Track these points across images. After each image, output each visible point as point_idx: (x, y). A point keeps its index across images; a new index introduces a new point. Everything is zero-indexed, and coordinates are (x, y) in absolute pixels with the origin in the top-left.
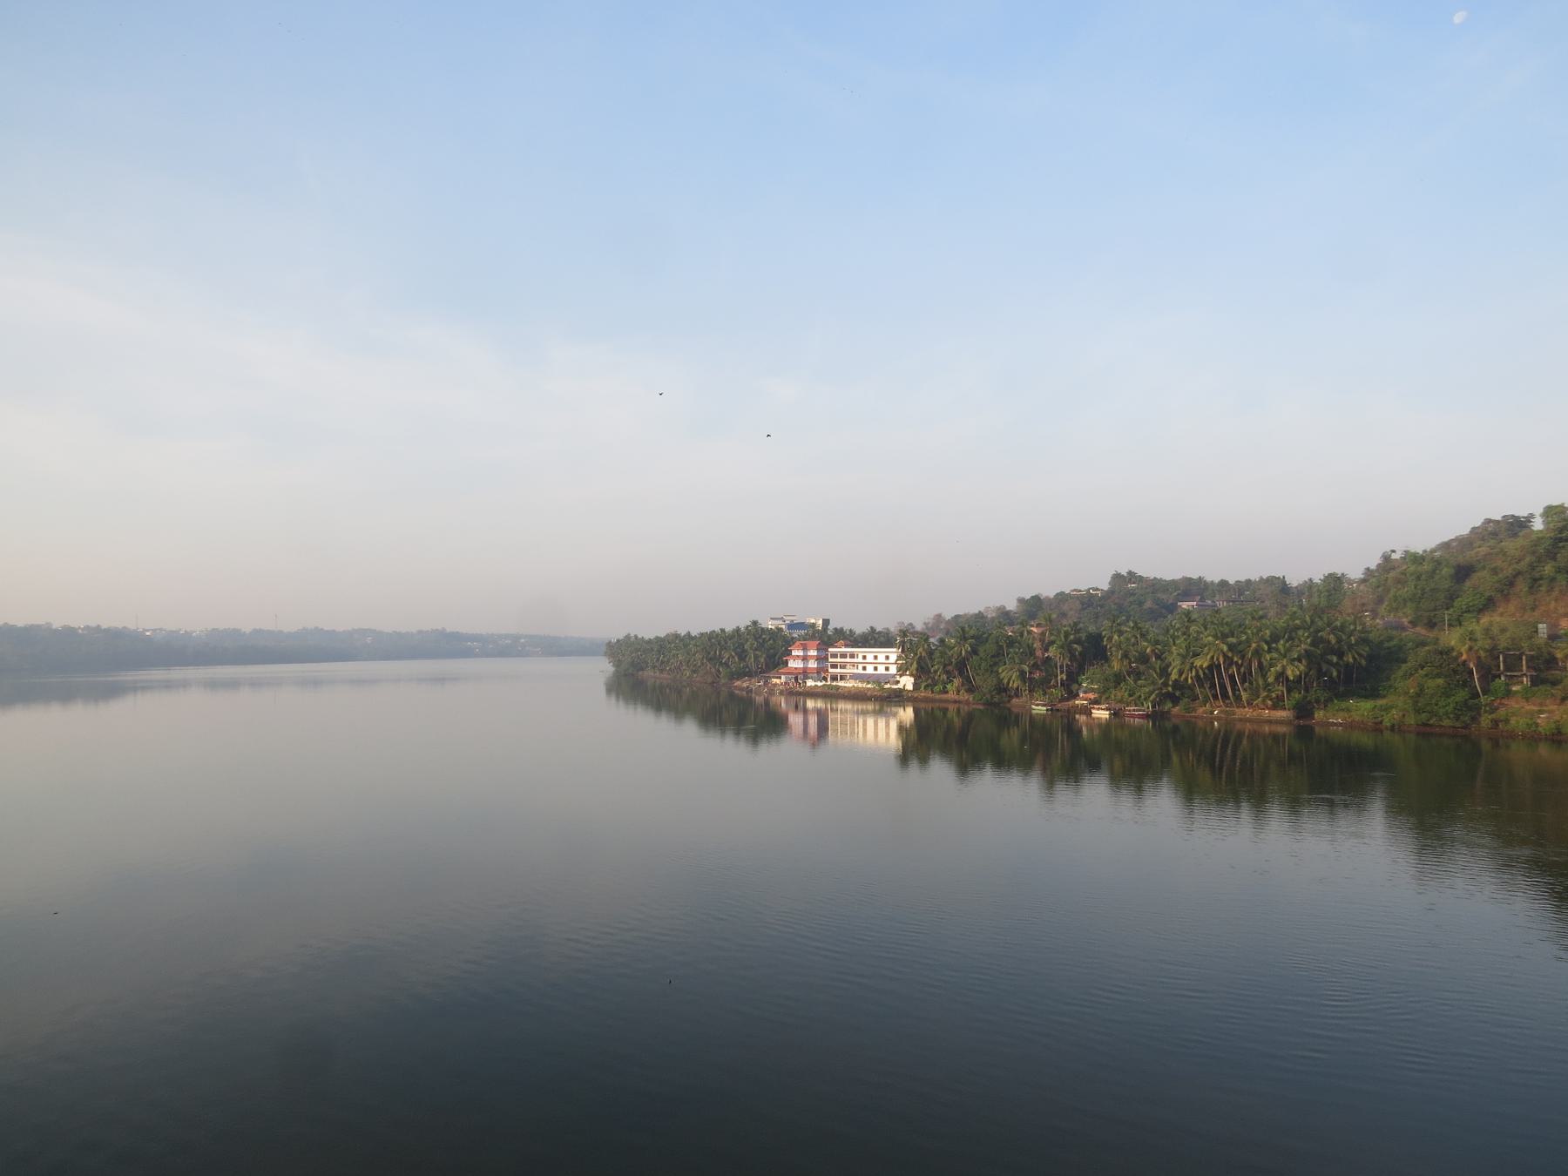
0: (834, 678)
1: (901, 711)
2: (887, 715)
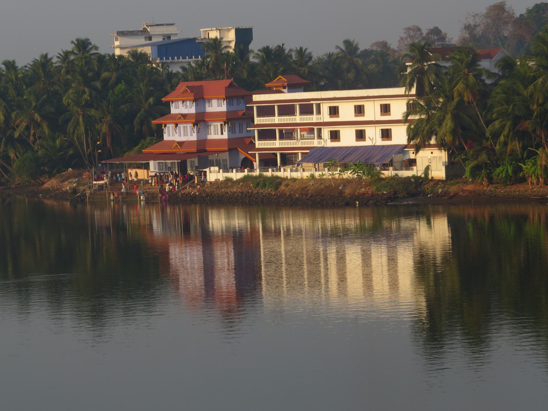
1: (422, 227)
2: (392, 238)
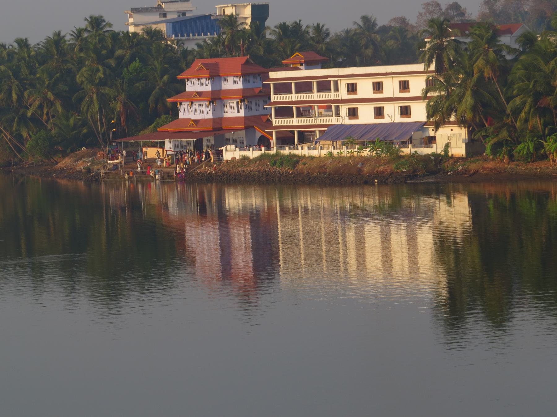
0: (286, 139)
1: (441, 206)
2: (409, 216)
